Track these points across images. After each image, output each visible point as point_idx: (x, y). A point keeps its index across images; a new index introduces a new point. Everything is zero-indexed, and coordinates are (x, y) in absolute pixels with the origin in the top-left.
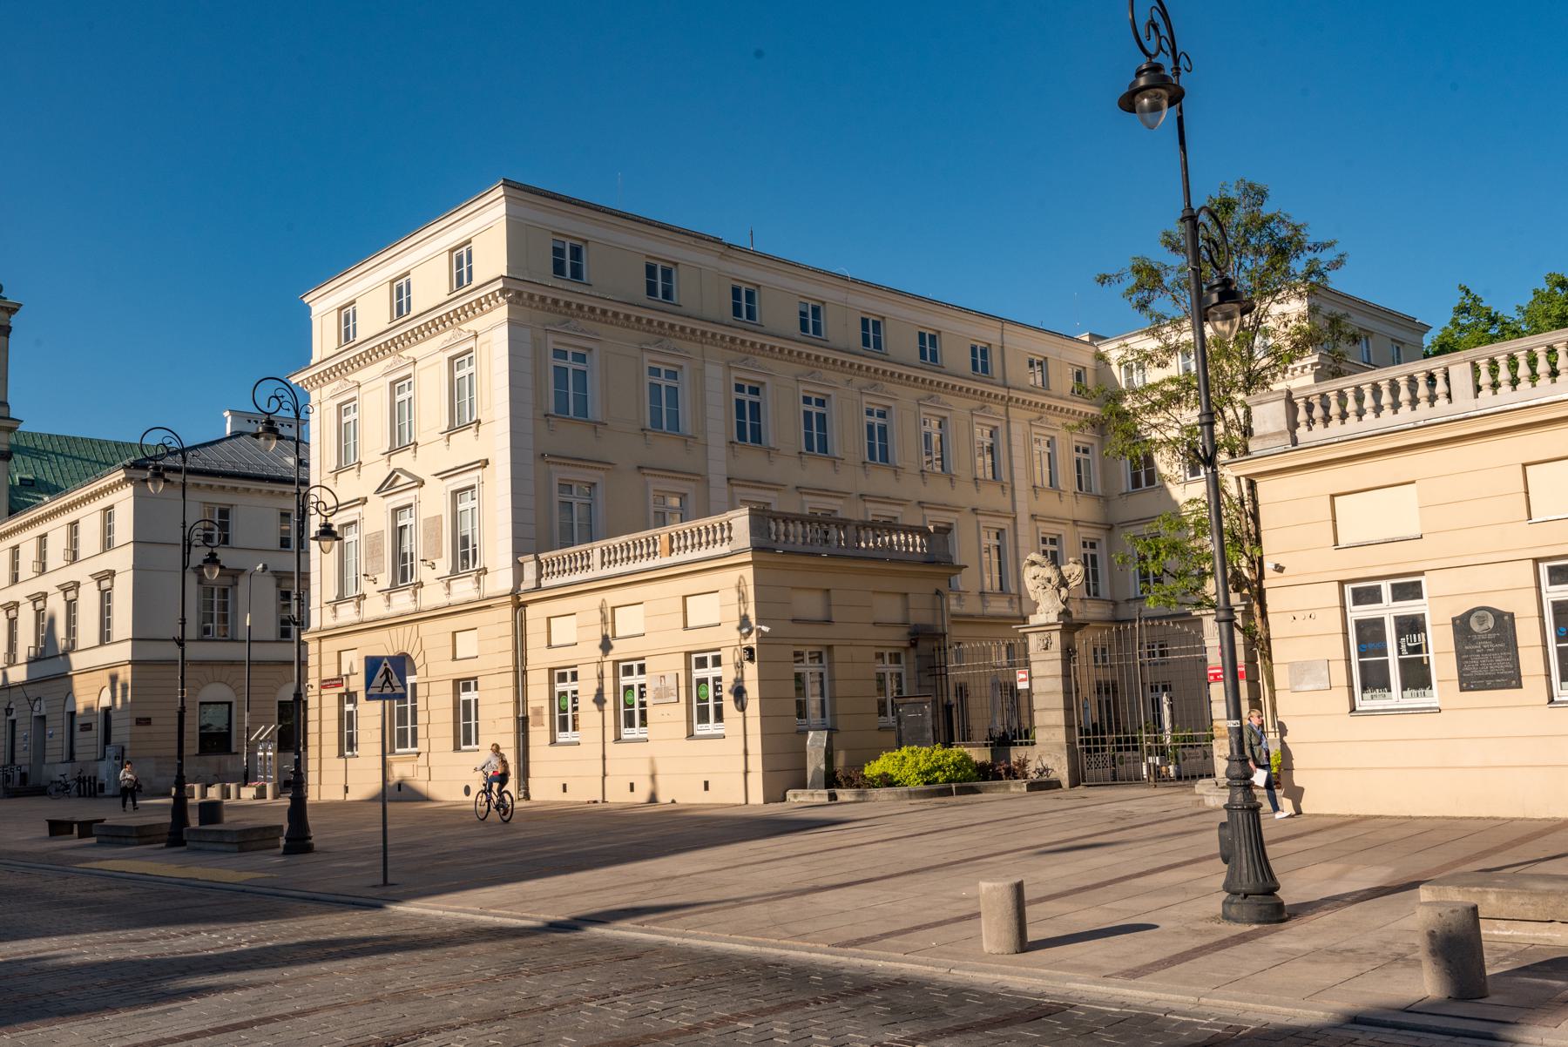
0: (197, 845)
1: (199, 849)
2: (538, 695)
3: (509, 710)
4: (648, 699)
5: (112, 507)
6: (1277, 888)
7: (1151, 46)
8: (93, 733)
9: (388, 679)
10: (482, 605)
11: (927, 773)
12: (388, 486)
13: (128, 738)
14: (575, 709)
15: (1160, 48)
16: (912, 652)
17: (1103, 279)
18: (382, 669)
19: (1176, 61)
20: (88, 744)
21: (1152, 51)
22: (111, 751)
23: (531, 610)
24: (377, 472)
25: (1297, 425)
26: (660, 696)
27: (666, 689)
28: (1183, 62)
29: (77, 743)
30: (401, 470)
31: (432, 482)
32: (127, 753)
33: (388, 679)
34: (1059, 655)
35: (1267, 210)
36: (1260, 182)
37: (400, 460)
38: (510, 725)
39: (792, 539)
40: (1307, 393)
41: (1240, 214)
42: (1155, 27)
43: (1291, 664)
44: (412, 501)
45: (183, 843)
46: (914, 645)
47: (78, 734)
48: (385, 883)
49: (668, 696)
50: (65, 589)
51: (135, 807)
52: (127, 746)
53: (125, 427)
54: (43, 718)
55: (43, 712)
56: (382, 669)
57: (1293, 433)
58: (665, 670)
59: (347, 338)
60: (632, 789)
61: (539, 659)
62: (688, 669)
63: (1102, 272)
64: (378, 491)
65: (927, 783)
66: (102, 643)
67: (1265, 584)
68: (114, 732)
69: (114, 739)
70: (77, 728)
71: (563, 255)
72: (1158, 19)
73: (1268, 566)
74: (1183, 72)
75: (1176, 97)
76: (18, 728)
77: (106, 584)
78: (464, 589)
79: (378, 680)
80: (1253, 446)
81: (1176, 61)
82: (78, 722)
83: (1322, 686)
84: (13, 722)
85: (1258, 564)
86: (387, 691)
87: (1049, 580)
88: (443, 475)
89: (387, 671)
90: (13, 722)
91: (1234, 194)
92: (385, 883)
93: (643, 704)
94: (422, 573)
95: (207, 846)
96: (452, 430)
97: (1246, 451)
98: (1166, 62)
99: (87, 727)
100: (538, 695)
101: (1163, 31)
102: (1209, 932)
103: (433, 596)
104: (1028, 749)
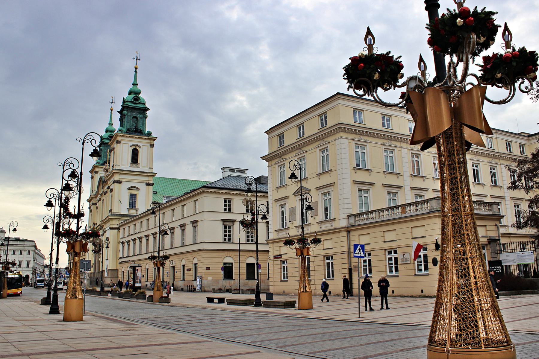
3: (346, 266)
27: (406, 259)
38: (347, 271)
50: (181, 226)
55: (174, 265)
79: (357, 252)
82: (186, 268)
86: (359, 255)
88: (318, 189)
99: (189, 270)
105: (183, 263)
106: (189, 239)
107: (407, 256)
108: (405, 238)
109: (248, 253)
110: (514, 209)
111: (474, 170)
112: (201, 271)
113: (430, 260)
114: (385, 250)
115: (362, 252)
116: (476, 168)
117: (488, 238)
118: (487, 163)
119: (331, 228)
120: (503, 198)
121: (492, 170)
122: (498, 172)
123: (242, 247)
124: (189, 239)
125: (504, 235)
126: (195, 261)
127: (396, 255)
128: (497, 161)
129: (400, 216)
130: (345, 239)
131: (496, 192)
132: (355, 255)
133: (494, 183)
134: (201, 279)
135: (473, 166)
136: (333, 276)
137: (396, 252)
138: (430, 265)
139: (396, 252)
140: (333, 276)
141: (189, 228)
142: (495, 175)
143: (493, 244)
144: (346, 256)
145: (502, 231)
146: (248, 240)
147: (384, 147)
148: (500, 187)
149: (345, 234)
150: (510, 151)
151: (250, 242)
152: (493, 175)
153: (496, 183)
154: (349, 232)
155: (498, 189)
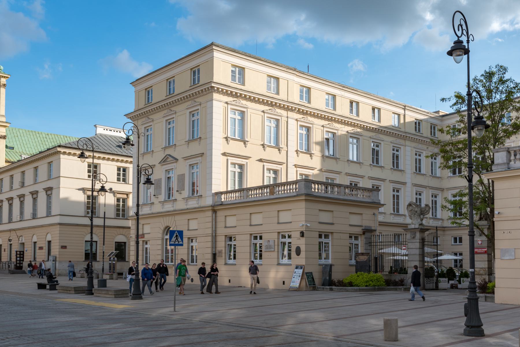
0: (98, 295)
1: (99, 296)
2: (221, 244)
3: (209, 251)
4: (263, 249)
5: (52, 162)
6: (482, 325)
7: (459, 34)
8: (43, 251)
9: (177, 239)
10: (200, 210)
11: (367, 282)
12: (164, 161)
13: (58, 253)
14: (235, 251)
15: (462, 33)
16: (363, 237)
17: (443, 100)
18: (175, 235)
19: (468, 38)
20: (41, 255)
21: (459, 35)
22: (51, 258)
23: (219, 213)
24: (161, 156)
25: (510, 161)
26: (267, 248)
27: (270, 246)
28: (471, 38)
29: (37, 254)
30: (170, 155)
31: (181, 160)
32: (57, 259)
33: (177, 239)
34: (418, 241)
35: (507, 76)
36: (505, 65)
37: (169, 152)
38: (210, 256)
39: (320, 191)
40: (515, 149)
41: (495, 79)
42: (461, 26)
43: (502, 250)
44: (173, 167)
45: (93, 294)
46: (364, 233)
47: (37, 251)
48: (175, 311)
49: (270, 248)
50: (32, 193)
51: (42, 278)
52: (58, 256)
53: (73, 137)
54: (23, 244)
55: (23, 241)
56: (175, 235)
57: (508, 164)
58: (270, 237)
59: (148, 102)
60: (230, 282)
61: (222, 231)
62: (278, 239)
63: (443, 97)
64: (160, 163)
65: (366, 286)
66: (47, 216)
67: (494, 219)
68: (52, 251)
69: (52, 253)
70: (37, 248)
71: (235, 74)
72: (463, 23)
73: (496, 212)
74: (470, 42)
75: (467, 52)
76: (13, 247)
77: (49, 193)
78: (193, 204)
79: (174, 239)
80: (494, 168)
81: (468, 38)
82: (38, 246)
83: (512, 258)
84: (11, 244)
85: (492, 211)
86: (177, 243)
87: (416, 212)
88: (186, 158)
89: (177, 236)
90: (11, 244)
91: (494, 70)
92: (175, 311)
93: (261, 251)
94: (176, 195)
95: (102, 295)
96: (189, 142)
97: (491, 170)
98: (464, 39)
99: (41, 248)
100: (221, 244)
101: (464, 27)
102: (457, 338)
103: (180, 205)
104: (405, 275)
105: (35, 239)
106: (42, 210)
107: (271, 243)
108: (265, 221)
109: (118, 230)
110: (392, 193)
111: (394, 154)
112: (55, 250)
113: (293, 249)
114: (251, 234)
115: (179, 239)
116: (376, 148)
117: (363, 228)
118: (390, 144)
119: (197, 206)
120: (404, 184)
121: (395, 152)
122: (401, 154)
123: (108, 223)
124: (42, 210)
125: (382, 224)
126: (49, 238)
127: (290, 240)
128: (402, 142)
129: (268, 197)
130: (210, 219)
131: (376, 173)
132: (172, 243)
133: (418, 170)
134: (55, 260)
135: (393, 150)
136: (196, 262)
137: (289, 237)
138: (293, 254)
139: (261, 238)
140: (196, 262)
141: (42, 198)
142: (397, 157)
143: (368, 235)
144: (210, 239)
145: (381, 218)
146: (118, 215)
147: (372, 140)
148: (401, 171)
149: (210, 213)
150: (419, 131)
151: (121, 217)
152: (396, 158)
153: (397, 167)
154: (215, 211)
155: (399, 173)
